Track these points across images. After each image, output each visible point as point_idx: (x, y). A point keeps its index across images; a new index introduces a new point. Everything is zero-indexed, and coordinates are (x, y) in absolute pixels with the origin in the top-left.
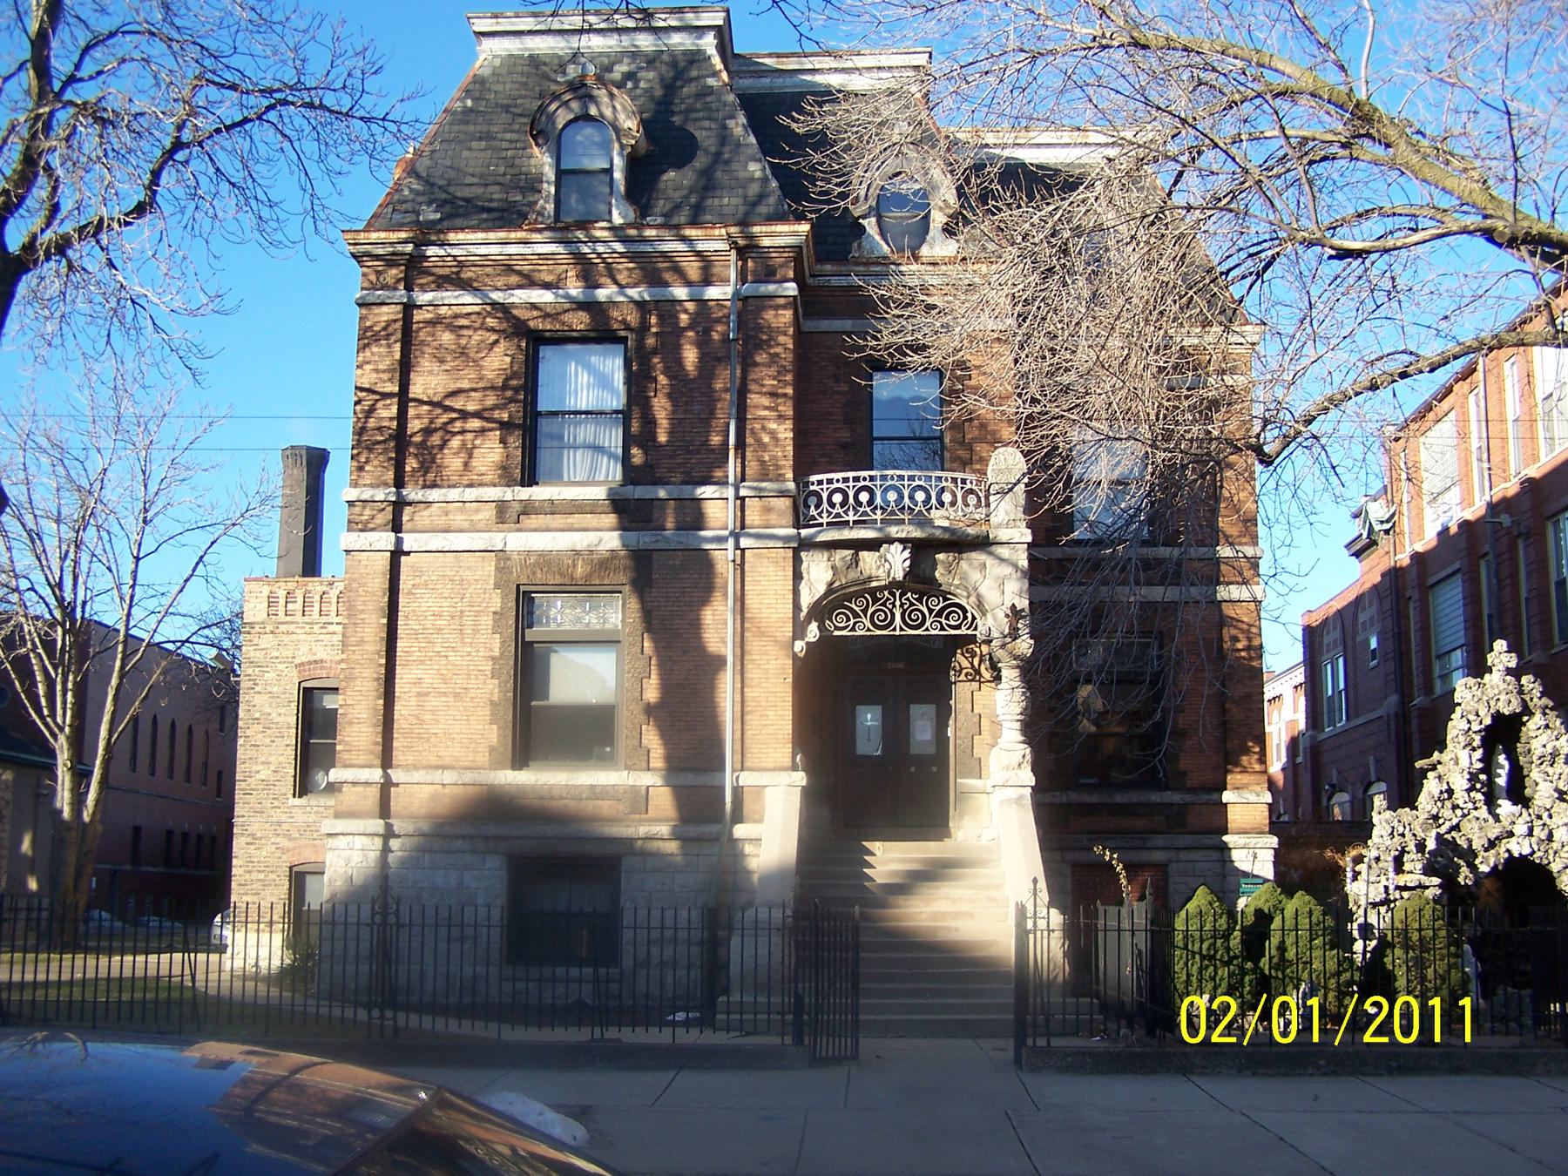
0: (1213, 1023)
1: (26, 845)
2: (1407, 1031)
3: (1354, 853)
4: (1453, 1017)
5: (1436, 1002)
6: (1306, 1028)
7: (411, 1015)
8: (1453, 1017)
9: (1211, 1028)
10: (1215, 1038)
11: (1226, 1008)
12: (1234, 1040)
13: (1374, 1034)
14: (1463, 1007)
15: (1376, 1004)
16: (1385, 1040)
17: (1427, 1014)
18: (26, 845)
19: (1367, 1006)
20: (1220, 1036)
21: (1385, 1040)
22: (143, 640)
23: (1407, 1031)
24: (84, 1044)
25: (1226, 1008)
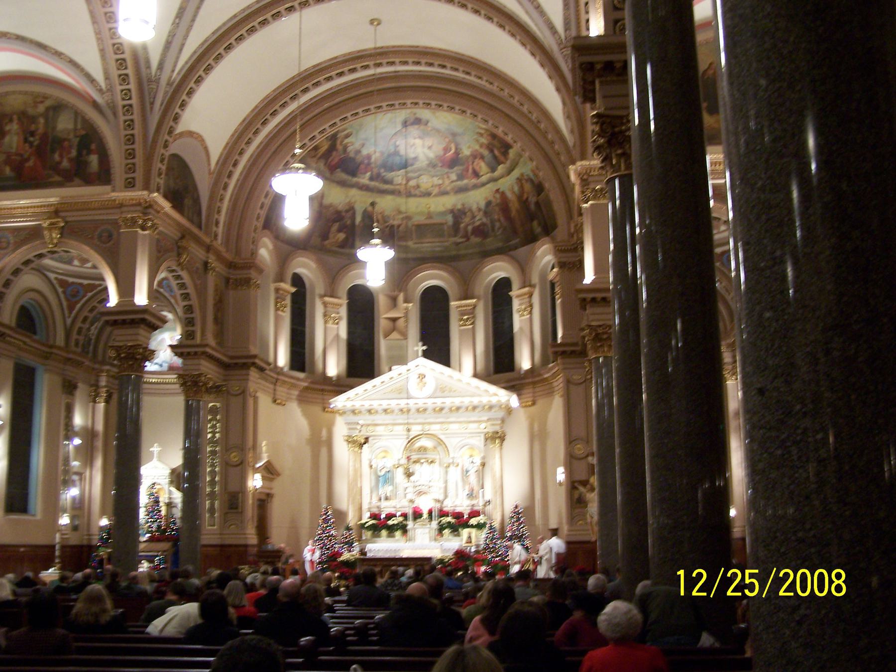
0: (792, 587)
10: (694, 593)
11: (700, 575)
12: (705, 594)
14: (680, 575)
16: (792, 594)
19: (781, 575)
20: (784, 592)
25: (700, 575)
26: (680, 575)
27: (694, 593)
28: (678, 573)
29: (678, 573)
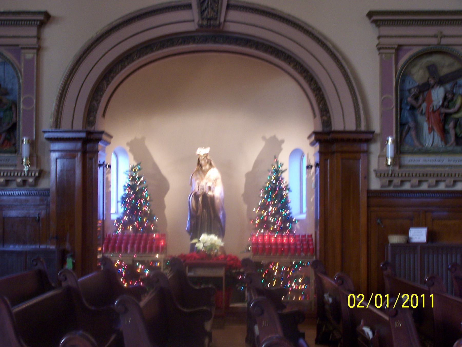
0: (408, 303)
1: (367, 330)
2: (414, 305)
3: (277, 205)
4: (428, 300)
5: (423, 296)
6: (385, 304)
7: (351, 126)
8: (428, 300)
9: (356, 304)
10: (358, 306)
13: (360, 305)
14: (431, 297)
15: (406, 296)
16: (408, 307)
17: (420, 299)
18: (367, 330)
19: (403, 297)
20: (360, 306)
21: (408, 307)
22: (221, 278)
23: (414, 305)
24: (429, 290)
26: (431, 297)
27: (358, 306)
28: (430, 296)
29: (430, 296)
